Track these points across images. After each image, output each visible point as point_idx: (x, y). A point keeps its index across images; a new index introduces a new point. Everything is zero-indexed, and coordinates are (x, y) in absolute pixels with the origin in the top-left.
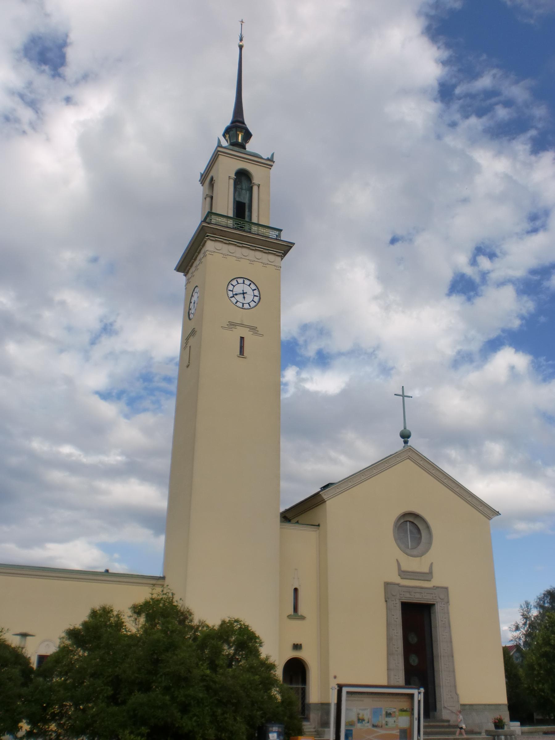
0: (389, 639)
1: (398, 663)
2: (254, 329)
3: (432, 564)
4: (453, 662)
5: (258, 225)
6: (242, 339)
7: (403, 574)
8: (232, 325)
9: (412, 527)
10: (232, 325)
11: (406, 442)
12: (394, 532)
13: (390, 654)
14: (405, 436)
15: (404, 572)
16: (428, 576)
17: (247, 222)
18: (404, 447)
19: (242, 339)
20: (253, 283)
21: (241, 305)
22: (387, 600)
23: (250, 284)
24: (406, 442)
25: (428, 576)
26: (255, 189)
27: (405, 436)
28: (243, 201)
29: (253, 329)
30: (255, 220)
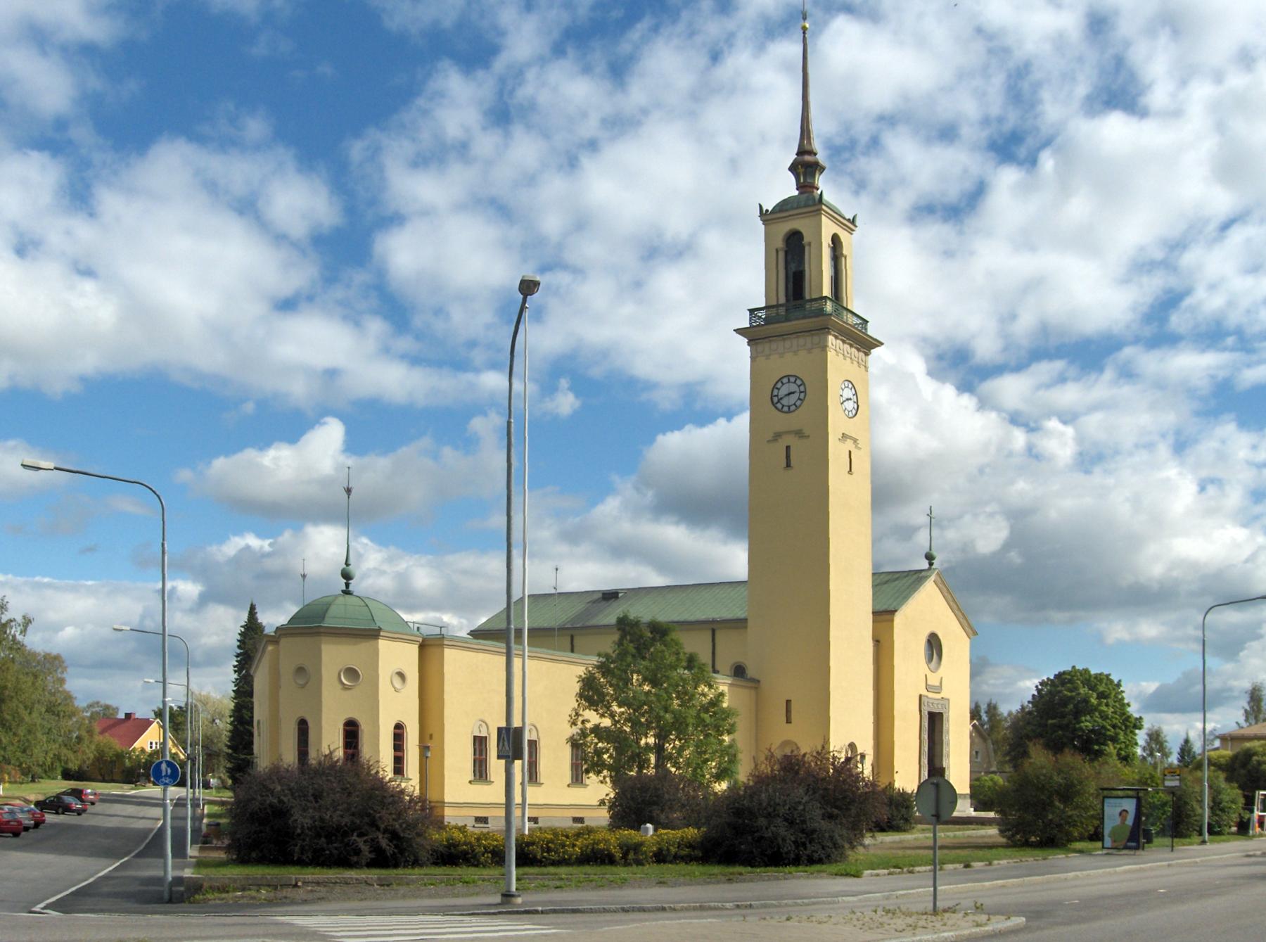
6: (788, 448)
8: (777, 436)
10: (777, 436)
19: (788, 448)
29: (799, 434)
30: (807, 297)
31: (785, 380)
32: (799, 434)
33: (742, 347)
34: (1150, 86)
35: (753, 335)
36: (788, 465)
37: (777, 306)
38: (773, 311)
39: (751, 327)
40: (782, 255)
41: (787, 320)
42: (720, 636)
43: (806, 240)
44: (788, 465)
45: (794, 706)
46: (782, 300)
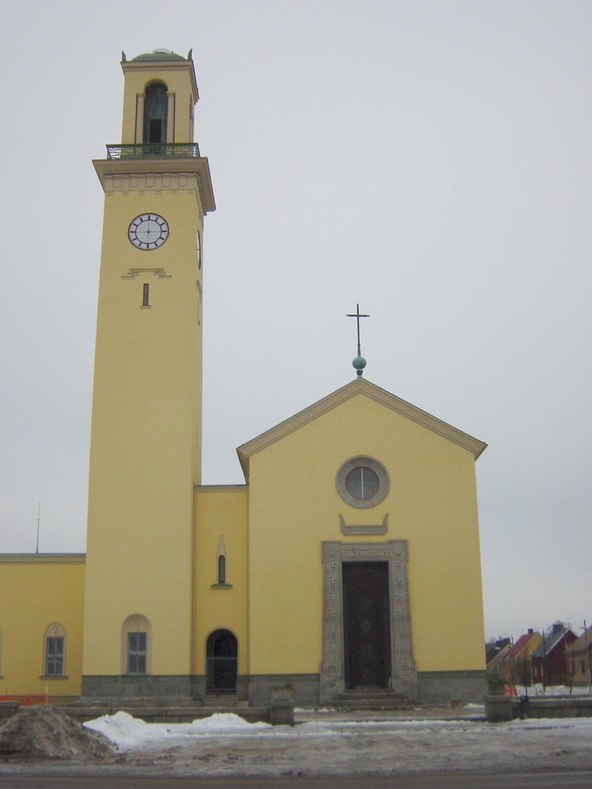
0: (326, 604)
1: (335, 564)
2: (161, 272)
3: (387, 516)
4: (410, 626)
5: (174, 145)
6: (146, 286)
7: (346, 529)
8: (134, 273)
9: (363, 477)
10: (134, 273)
11: (360, 373)
12: (337, 475)
13: (326, 620)
14: (360, 365)
15: (347, 527)
16: (383, 528)
17: (163, 144)
18: (358, 378)
19: (146, 286)
20: (142, 215)
21: (161, 241)
22: (324, 561)
23: (141, 219)
24: (360, 373)
25: (383, 528)
26: (171, 100)
27: (360, 365)
28: (158, 118)
29: (160, 273)
30: (169, 140)
31: (133, 236)
32: (160, 273)
33: (94, 192)
34: (559, 622)
35: (107, 171)
36: (146, 303)
37: (135, 145)
38: (130, 151)
39: (110, 159)
40: (141, 100)
41: (143, 158)
42: (136, 237)
43: (170, 90)
44: (146, 303)
45: (359, 305)
46: (140, 141)
